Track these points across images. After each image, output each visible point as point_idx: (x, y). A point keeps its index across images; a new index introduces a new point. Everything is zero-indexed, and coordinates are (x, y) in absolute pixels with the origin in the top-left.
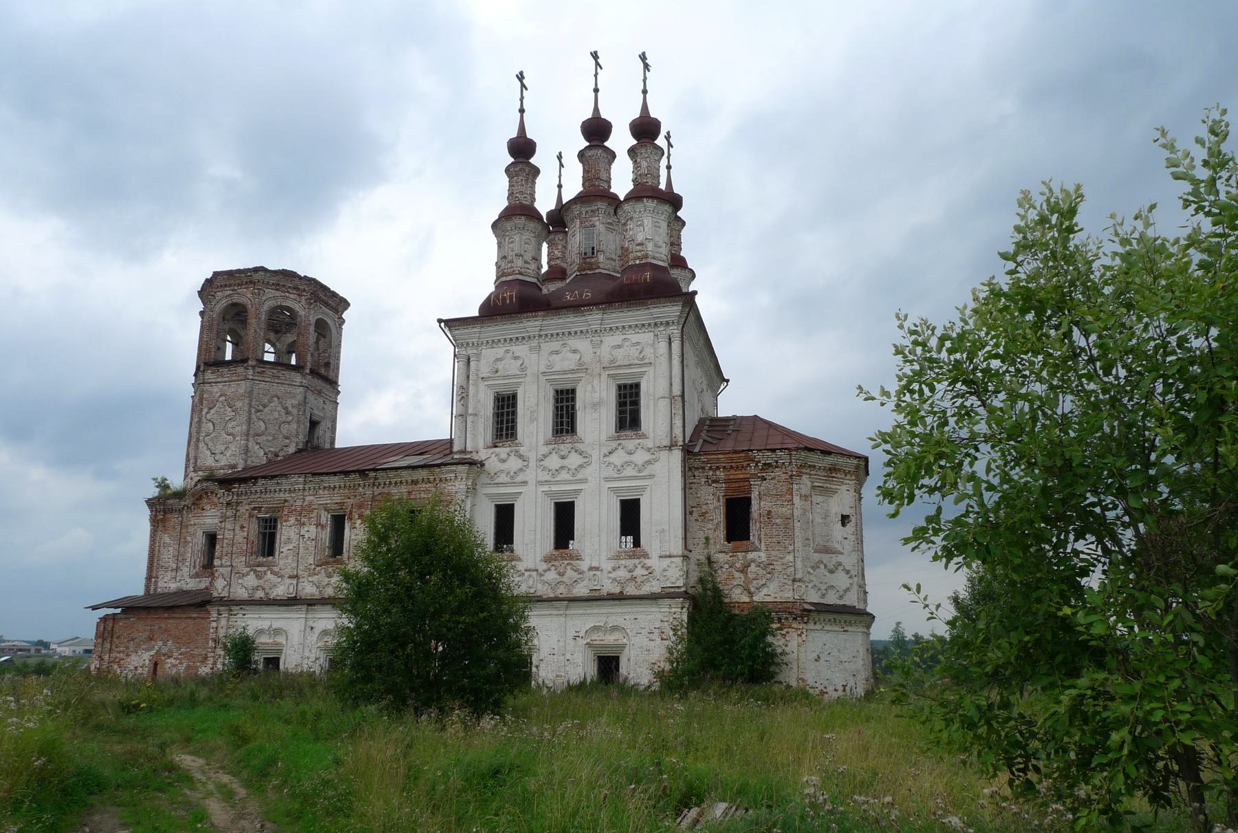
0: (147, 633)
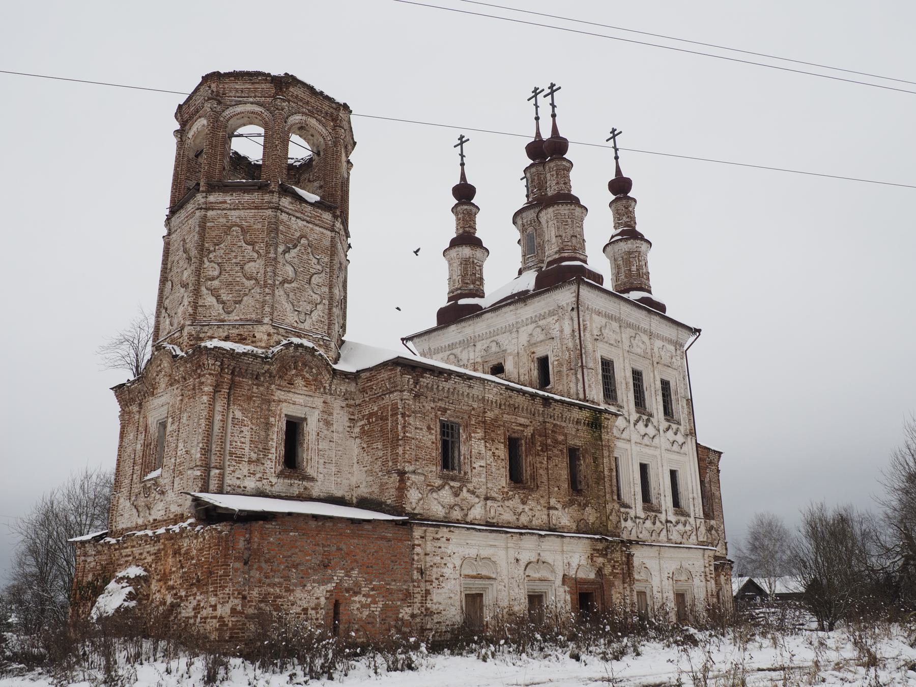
0: (320, 558)
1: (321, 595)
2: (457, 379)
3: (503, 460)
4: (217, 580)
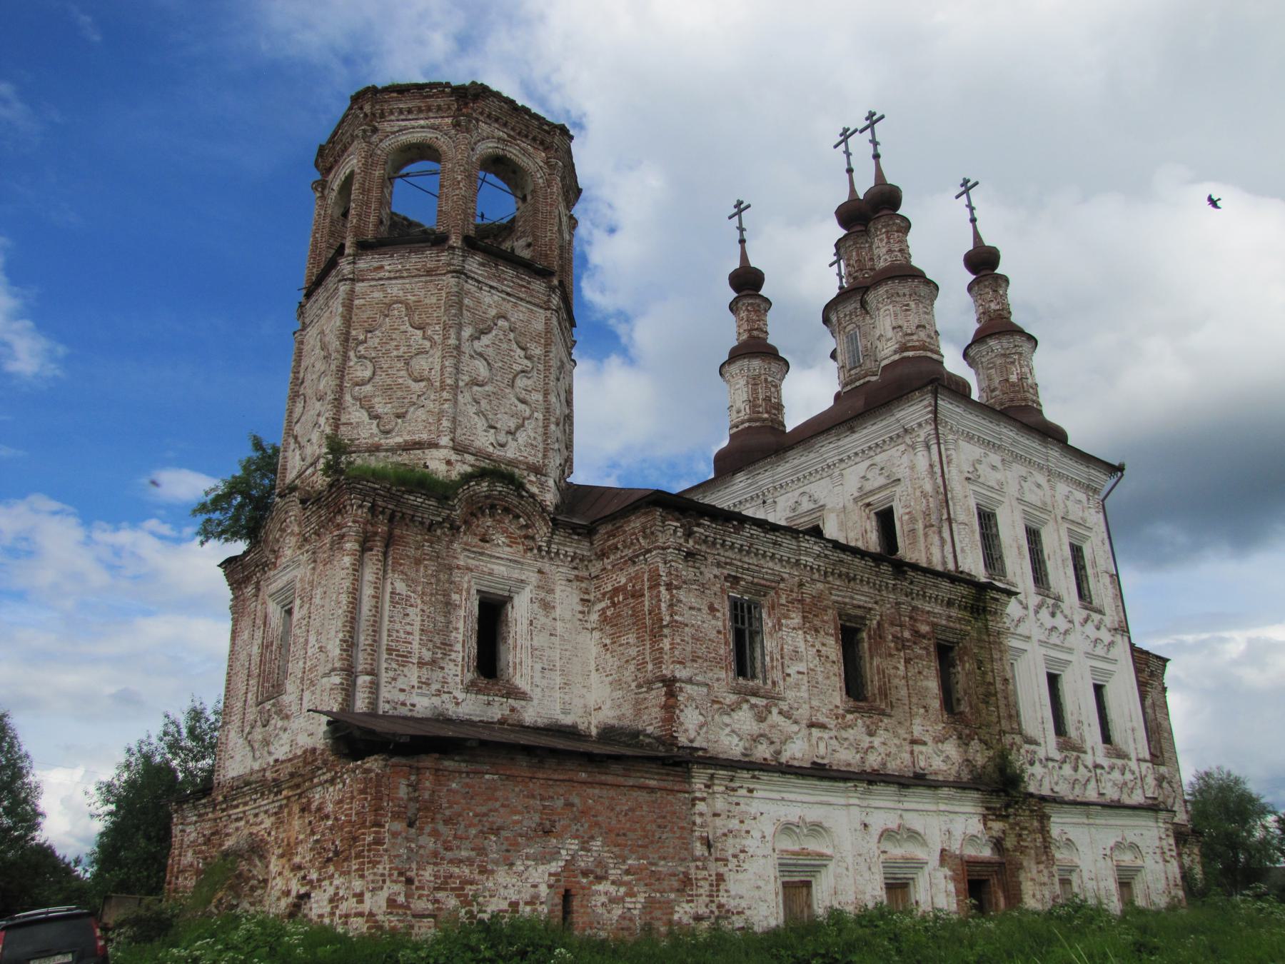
0: (536, 818)
1: (541, 880)
2: (756, 531)
3: (834, 662)
4: (363, 851)
